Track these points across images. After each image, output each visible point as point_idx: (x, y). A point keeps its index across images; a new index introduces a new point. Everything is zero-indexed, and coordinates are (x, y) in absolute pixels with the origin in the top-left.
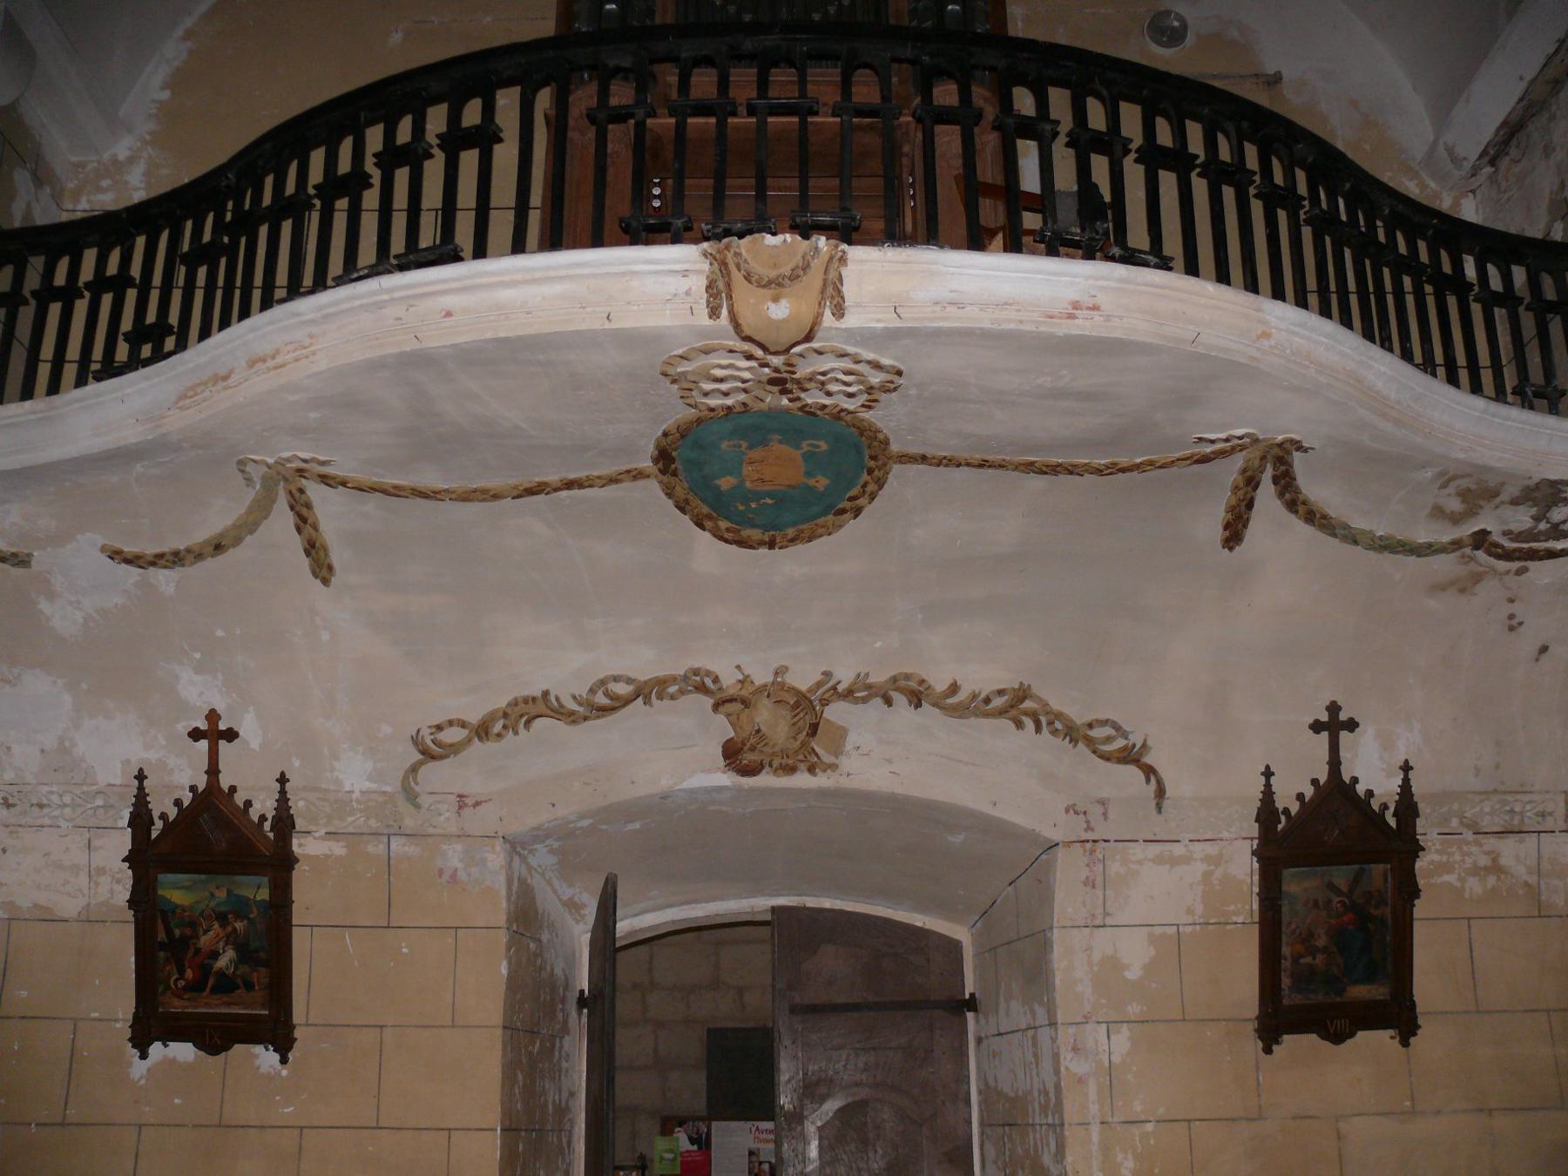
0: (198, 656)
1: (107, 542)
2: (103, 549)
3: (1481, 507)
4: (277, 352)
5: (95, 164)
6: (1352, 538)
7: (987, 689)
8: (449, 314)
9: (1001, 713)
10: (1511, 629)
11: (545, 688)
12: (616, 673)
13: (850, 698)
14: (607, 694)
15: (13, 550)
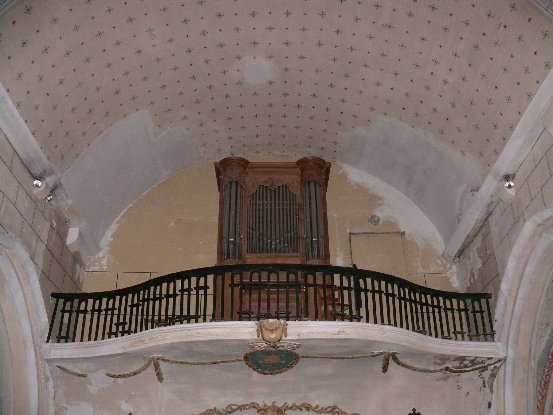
0: (127, 399)
1: (107, 372)
2: (106, 374)
3: (446, 362)
4: (157, 337)
5: (94, 258)
6: (415, 370)
7: (326, 406)
8: (198, 333)
9: (329, 412)
10: (459, 389)
11: (215, 407)
12: (233, 403)
13: (291, 409)
14: (231, 409)
15: (83, 373)
